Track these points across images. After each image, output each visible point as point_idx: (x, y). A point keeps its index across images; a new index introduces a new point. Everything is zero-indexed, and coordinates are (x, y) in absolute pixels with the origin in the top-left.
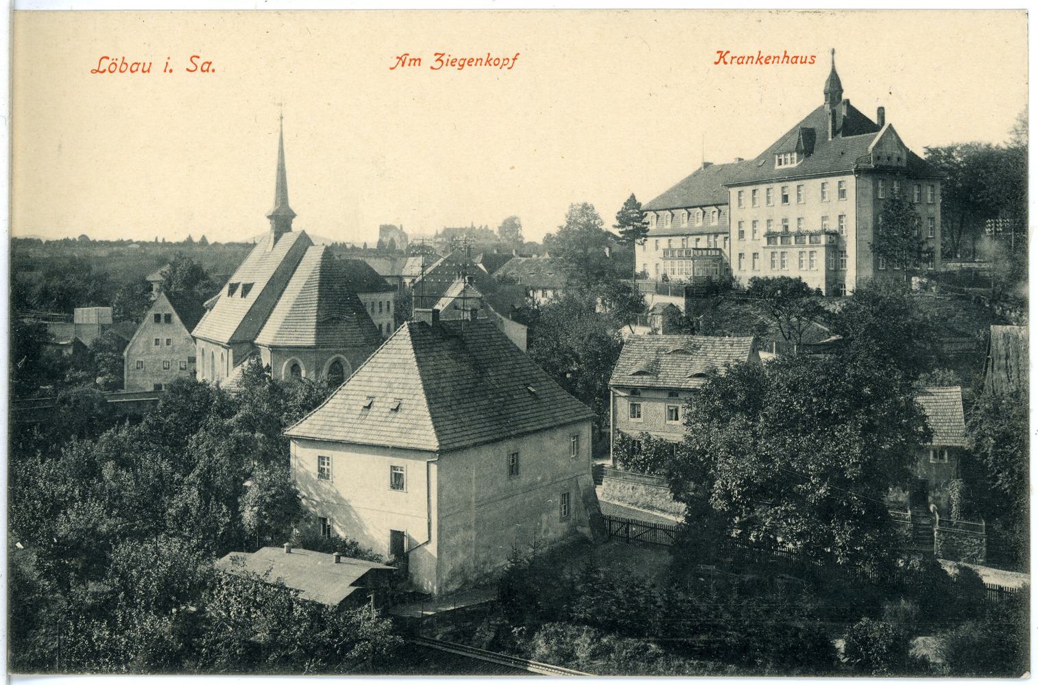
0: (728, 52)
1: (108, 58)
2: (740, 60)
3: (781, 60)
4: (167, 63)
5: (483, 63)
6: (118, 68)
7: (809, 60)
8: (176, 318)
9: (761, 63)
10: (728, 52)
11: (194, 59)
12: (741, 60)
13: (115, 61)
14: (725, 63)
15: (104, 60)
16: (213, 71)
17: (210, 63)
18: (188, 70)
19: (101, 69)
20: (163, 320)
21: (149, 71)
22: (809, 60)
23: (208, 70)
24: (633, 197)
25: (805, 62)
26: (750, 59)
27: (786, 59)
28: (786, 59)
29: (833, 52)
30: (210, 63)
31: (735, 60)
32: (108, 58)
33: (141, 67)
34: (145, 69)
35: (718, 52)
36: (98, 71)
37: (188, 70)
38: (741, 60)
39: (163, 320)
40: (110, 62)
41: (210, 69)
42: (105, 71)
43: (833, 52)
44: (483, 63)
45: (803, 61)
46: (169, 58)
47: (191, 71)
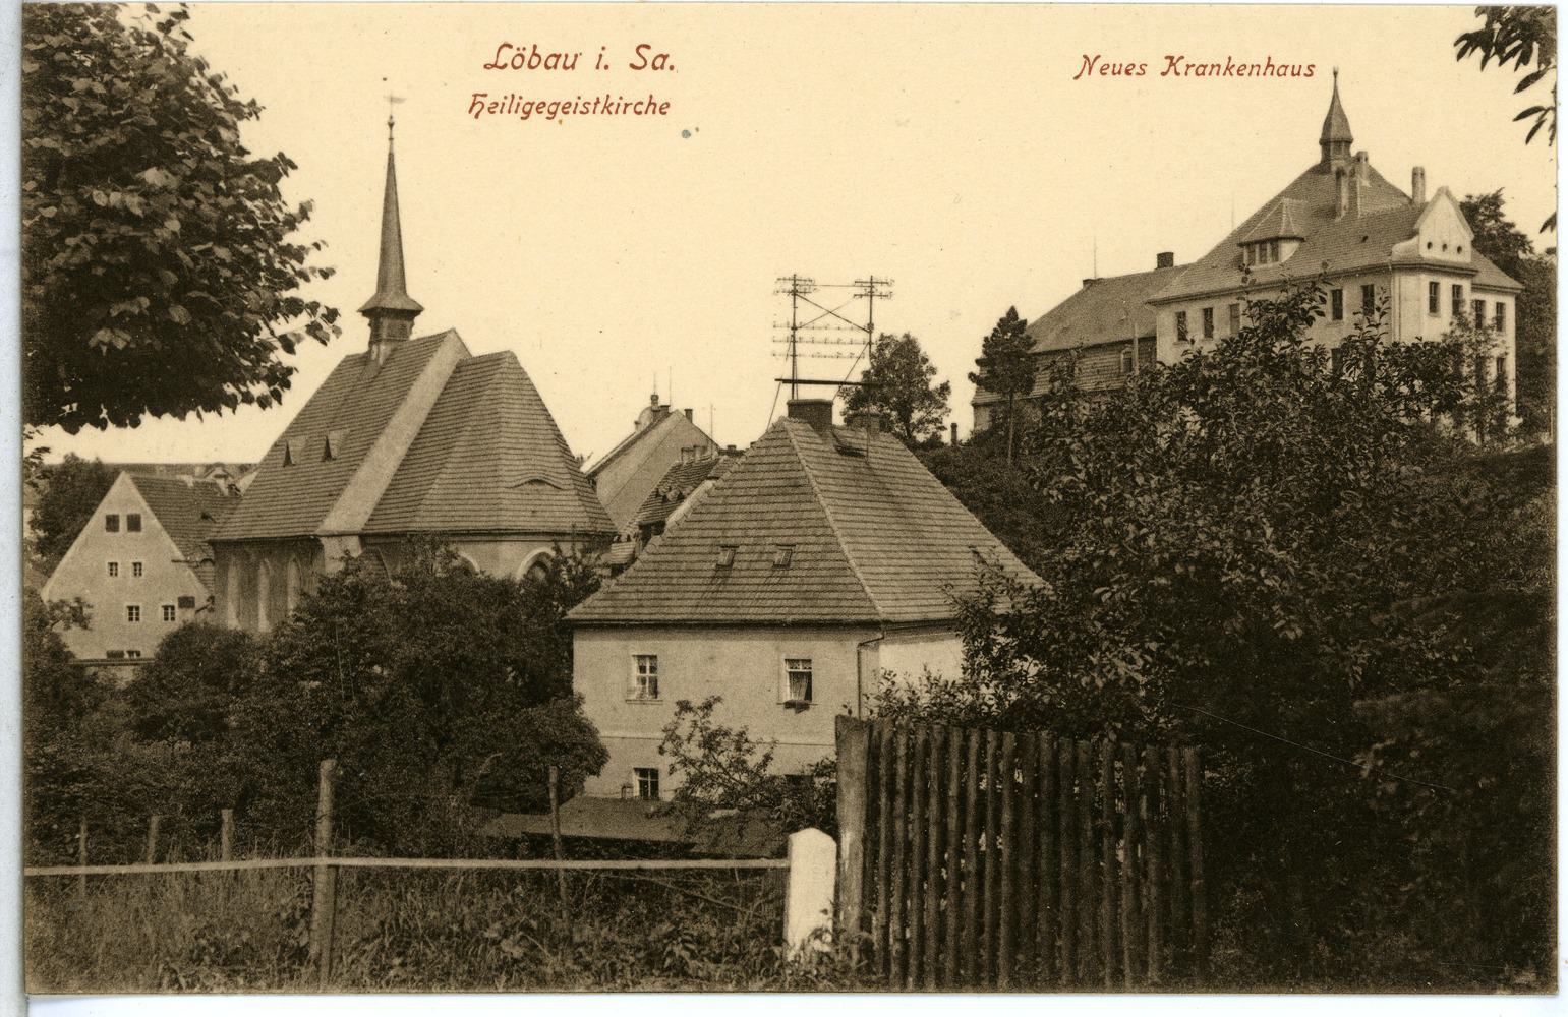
0: (1182, 57)
1: (510, 46)
2: (1201, 70)
3: (1262, 71)
4: (601, 56)
5: (1222, 71)
6: (526, 63)
7: (1304, 70)
8: (150, 521)
9: (610, 113)
10: (1182, 57)
11: (643, 51)
12: (1201, 70)
13: (521, 51)
14: (1177, 74)
15: (505, 49)
16: (671, 68)
17: (665, 57)
18: (632, 66)
19: (500, 64)
20: (123, 524)
21: (573, 66)
22: (1304, 70)
23: (662, 67)
24: (1013, 313)
25: (1299, 74)
26: (1216, 69)
27: (652, 107)
28: (652, 107)
29: (1335, 74)
30: (665, 57)
31: (1192, 70)
32: (510, 46)
33: (1289, 71)
34: (568, 64)
35: (1167, 58)
36: (495, 66)
37: (632, 66)
38: (1201, 70)
39: (123, 524)
40: (514, 52)
41: (667, 66)
42: (505, 66)
43: (1335, 74)
44: (1222, 71)
45: (1216, 69)
46: (604, 48)
47: (640, 68)
